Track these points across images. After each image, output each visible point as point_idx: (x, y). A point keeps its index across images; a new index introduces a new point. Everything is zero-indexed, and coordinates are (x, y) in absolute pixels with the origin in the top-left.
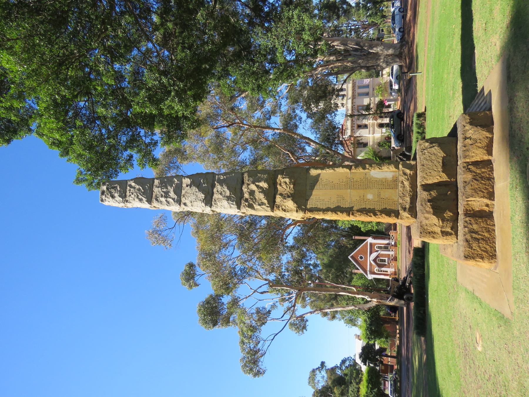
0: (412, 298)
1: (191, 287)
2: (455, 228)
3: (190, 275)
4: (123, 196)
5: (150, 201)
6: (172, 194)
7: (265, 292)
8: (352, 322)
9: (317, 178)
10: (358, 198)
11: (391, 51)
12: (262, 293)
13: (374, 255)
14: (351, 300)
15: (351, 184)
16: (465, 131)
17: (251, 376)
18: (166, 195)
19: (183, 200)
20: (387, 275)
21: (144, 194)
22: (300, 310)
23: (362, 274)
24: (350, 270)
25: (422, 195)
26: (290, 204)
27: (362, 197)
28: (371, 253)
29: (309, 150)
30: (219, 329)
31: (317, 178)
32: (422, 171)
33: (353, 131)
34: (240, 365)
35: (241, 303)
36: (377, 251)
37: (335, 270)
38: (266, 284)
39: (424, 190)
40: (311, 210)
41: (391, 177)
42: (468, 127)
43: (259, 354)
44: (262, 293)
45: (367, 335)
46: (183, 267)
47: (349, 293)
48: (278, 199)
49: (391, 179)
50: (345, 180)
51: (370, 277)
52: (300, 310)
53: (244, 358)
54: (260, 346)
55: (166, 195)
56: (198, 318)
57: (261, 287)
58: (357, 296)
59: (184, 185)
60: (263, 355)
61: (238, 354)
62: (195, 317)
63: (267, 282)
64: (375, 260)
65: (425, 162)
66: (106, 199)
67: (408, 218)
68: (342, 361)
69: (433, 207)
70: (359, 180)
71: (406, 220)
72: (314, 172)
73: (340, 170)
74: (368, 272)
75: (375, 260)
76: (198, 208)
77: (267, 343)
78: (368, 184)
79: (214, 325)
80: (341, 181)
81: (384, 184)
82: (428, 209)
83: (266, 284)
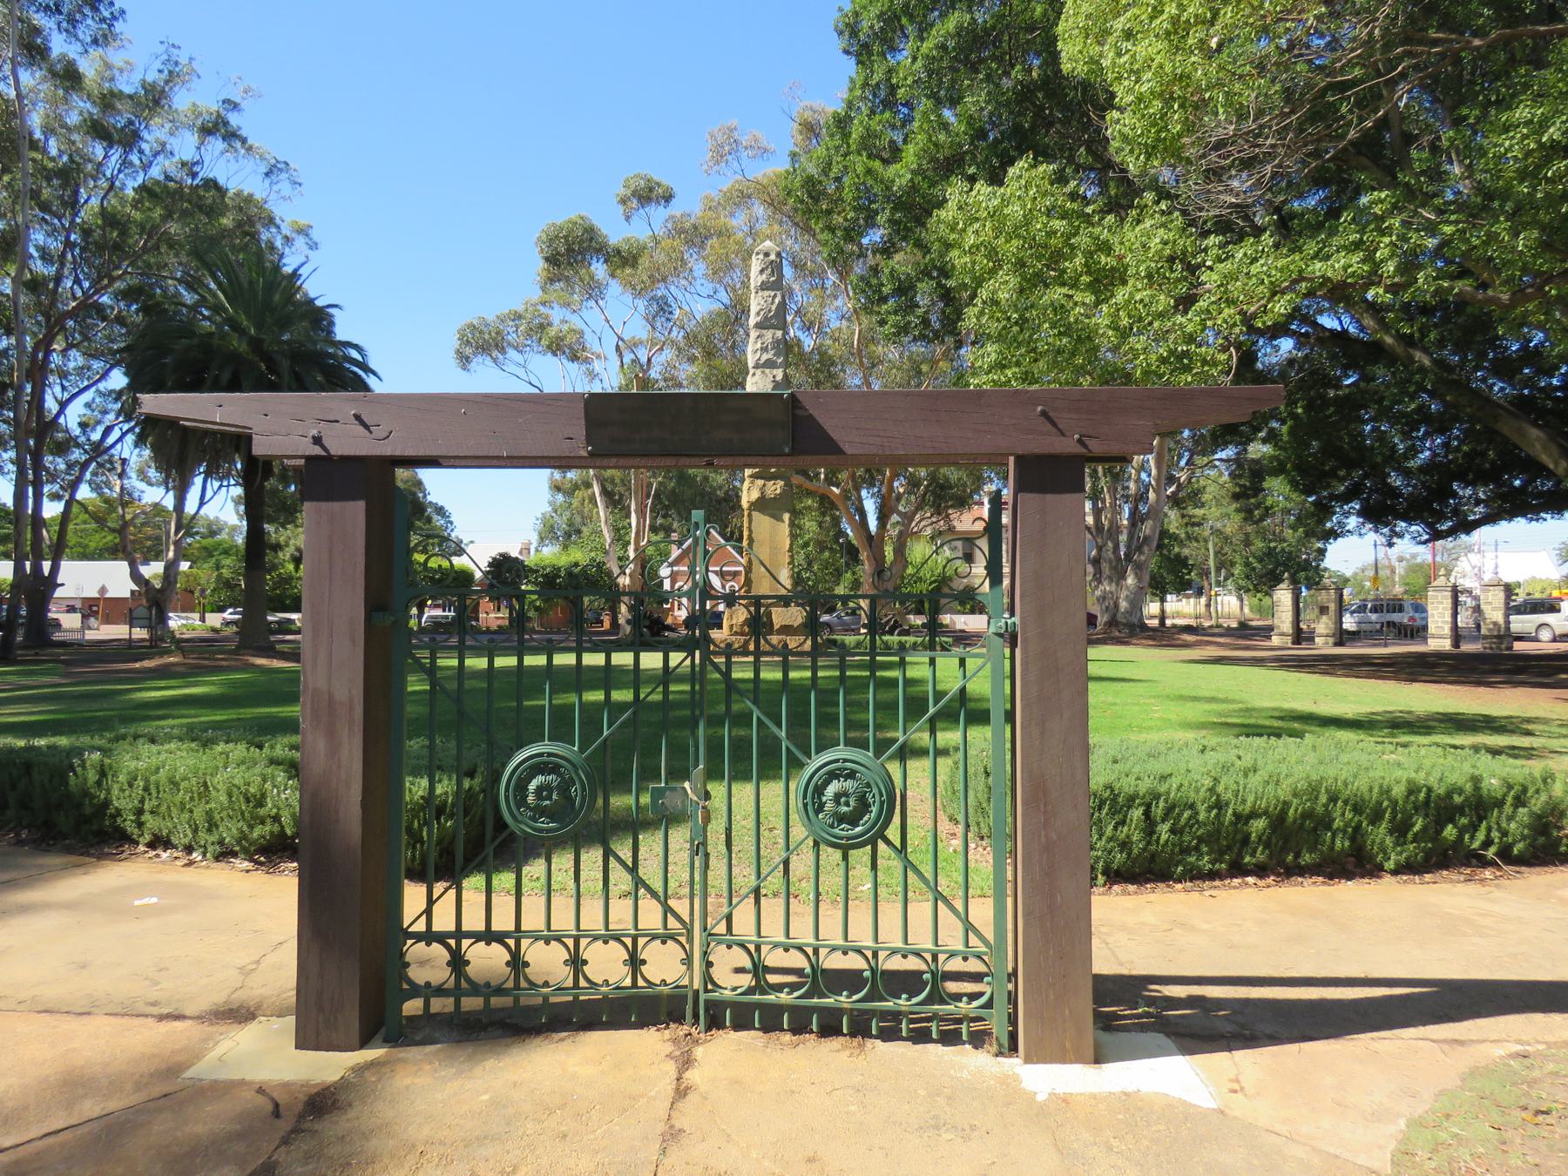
1: (623, 201)
2: (736, 633)
3: (647, 194)
4: (764, 287)
5: (758, 326)
6: (765, 357)
7: (621, 356)
8: (548, 532)
9: (781, 520)
11: (1123, 605)
14: (620, 536)
17: (457, 344)
18: (764, 349)
19: (758, 372)
21: (766, 318)
23: (668, 554)
24: (675, 525)
26: (755, 495)
30: (537, 265)
31: (781, 520)
34: (470, 317)
35: (592, 303)
37: (673, 491)
40: (750, 515)
43: (495, 353)
45: (544, 568)
46: (664, 178)
47: (637, 533)
48: (760, 482)
53: (487, 325)
54: (512, 353)
55: (764, 349)
56: (560, 221)
58: (631, 548)
59: (775, 371)
60: (495, 360)
61: (490, 308)
62: (563, 213)
68: (442, 508)
72: (786, 516)
73: (788, 542)
77: (521, 372)
79: (547, 259)
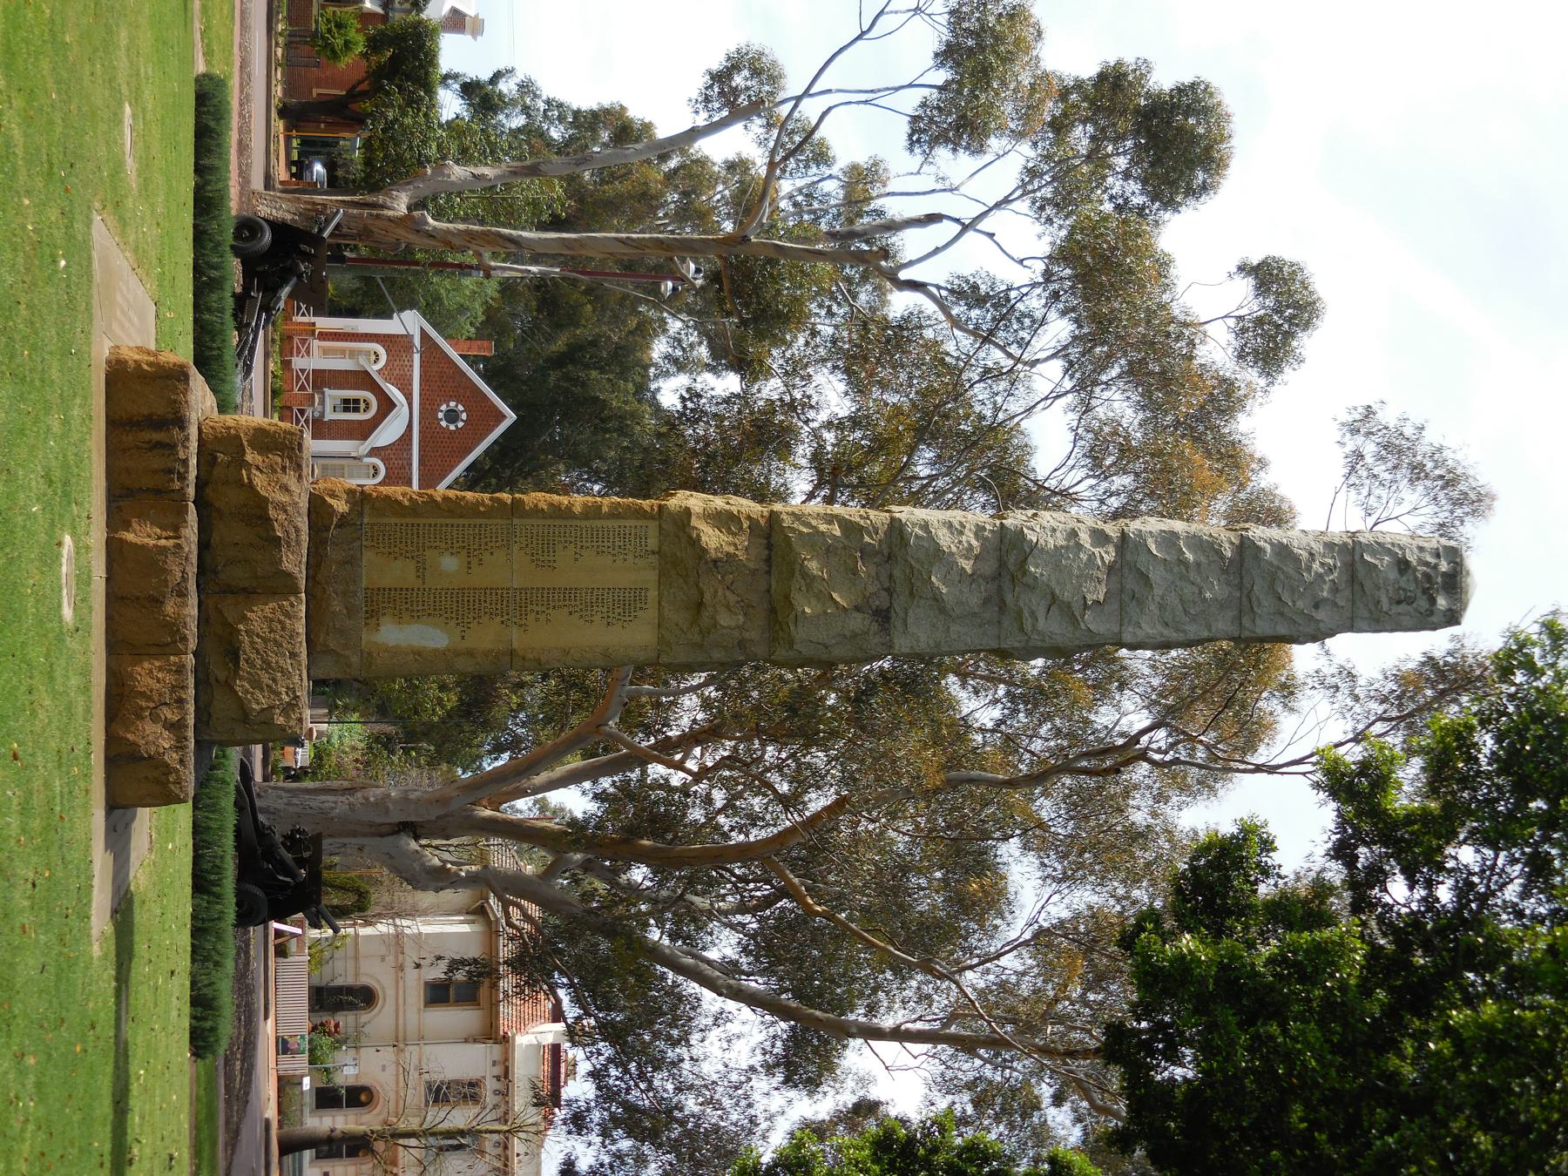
0: (237, 235)
10: (486, 556)
12: (933, 218)
13: (388, 433)
15: (515, 604)
16: (180, 747)
20: (325, 336)
22: (738, 143)
25: (295, 562)
27: (475, 561)
28: (406, 437)
29: (723, 946)
32: (293, 635)
33: (498, 1070)
36: (374, 452)
38: (911, 263)
39: (289, 575)
41: (382, 628)
42: (172, 758)
44: (933, 218)
49: (383, 620)
50: (531, 617)
51: (409, 323)
52: (738, 143)
57: (937, 250)
63: (903, 275)
64: (387, 405)
65: (287, 663)
66: (1433, 561)
67: (333, 495)
69: (267, 521)
70: (485, 619)
71: (339, 490)
74: (417, 341)
75: (387, 405)
76: (1054, 524)
78: (459, 605)
80: (542, 617)
81: (406, 604)
82: (282, 517)
83: (911, 263)
